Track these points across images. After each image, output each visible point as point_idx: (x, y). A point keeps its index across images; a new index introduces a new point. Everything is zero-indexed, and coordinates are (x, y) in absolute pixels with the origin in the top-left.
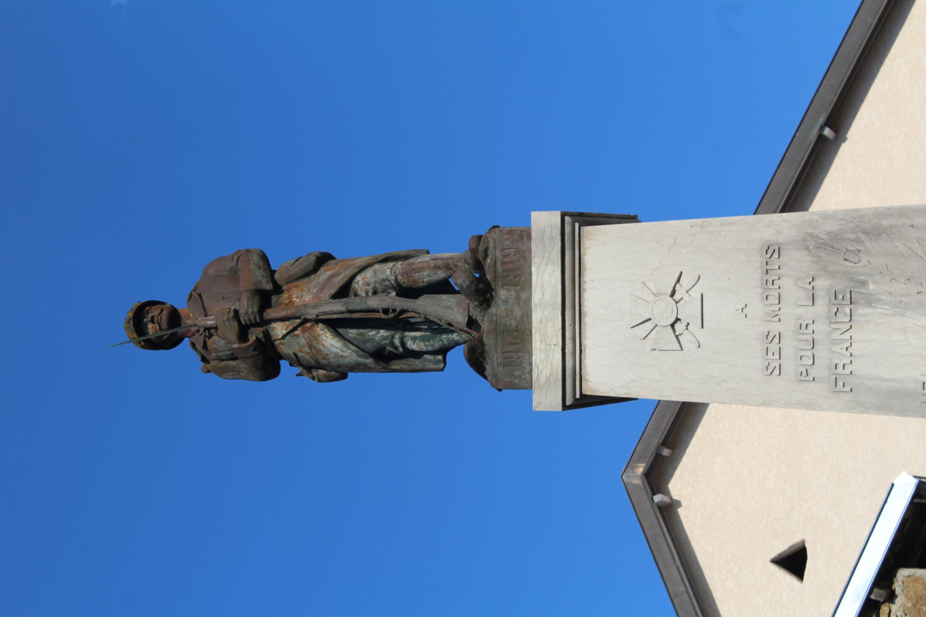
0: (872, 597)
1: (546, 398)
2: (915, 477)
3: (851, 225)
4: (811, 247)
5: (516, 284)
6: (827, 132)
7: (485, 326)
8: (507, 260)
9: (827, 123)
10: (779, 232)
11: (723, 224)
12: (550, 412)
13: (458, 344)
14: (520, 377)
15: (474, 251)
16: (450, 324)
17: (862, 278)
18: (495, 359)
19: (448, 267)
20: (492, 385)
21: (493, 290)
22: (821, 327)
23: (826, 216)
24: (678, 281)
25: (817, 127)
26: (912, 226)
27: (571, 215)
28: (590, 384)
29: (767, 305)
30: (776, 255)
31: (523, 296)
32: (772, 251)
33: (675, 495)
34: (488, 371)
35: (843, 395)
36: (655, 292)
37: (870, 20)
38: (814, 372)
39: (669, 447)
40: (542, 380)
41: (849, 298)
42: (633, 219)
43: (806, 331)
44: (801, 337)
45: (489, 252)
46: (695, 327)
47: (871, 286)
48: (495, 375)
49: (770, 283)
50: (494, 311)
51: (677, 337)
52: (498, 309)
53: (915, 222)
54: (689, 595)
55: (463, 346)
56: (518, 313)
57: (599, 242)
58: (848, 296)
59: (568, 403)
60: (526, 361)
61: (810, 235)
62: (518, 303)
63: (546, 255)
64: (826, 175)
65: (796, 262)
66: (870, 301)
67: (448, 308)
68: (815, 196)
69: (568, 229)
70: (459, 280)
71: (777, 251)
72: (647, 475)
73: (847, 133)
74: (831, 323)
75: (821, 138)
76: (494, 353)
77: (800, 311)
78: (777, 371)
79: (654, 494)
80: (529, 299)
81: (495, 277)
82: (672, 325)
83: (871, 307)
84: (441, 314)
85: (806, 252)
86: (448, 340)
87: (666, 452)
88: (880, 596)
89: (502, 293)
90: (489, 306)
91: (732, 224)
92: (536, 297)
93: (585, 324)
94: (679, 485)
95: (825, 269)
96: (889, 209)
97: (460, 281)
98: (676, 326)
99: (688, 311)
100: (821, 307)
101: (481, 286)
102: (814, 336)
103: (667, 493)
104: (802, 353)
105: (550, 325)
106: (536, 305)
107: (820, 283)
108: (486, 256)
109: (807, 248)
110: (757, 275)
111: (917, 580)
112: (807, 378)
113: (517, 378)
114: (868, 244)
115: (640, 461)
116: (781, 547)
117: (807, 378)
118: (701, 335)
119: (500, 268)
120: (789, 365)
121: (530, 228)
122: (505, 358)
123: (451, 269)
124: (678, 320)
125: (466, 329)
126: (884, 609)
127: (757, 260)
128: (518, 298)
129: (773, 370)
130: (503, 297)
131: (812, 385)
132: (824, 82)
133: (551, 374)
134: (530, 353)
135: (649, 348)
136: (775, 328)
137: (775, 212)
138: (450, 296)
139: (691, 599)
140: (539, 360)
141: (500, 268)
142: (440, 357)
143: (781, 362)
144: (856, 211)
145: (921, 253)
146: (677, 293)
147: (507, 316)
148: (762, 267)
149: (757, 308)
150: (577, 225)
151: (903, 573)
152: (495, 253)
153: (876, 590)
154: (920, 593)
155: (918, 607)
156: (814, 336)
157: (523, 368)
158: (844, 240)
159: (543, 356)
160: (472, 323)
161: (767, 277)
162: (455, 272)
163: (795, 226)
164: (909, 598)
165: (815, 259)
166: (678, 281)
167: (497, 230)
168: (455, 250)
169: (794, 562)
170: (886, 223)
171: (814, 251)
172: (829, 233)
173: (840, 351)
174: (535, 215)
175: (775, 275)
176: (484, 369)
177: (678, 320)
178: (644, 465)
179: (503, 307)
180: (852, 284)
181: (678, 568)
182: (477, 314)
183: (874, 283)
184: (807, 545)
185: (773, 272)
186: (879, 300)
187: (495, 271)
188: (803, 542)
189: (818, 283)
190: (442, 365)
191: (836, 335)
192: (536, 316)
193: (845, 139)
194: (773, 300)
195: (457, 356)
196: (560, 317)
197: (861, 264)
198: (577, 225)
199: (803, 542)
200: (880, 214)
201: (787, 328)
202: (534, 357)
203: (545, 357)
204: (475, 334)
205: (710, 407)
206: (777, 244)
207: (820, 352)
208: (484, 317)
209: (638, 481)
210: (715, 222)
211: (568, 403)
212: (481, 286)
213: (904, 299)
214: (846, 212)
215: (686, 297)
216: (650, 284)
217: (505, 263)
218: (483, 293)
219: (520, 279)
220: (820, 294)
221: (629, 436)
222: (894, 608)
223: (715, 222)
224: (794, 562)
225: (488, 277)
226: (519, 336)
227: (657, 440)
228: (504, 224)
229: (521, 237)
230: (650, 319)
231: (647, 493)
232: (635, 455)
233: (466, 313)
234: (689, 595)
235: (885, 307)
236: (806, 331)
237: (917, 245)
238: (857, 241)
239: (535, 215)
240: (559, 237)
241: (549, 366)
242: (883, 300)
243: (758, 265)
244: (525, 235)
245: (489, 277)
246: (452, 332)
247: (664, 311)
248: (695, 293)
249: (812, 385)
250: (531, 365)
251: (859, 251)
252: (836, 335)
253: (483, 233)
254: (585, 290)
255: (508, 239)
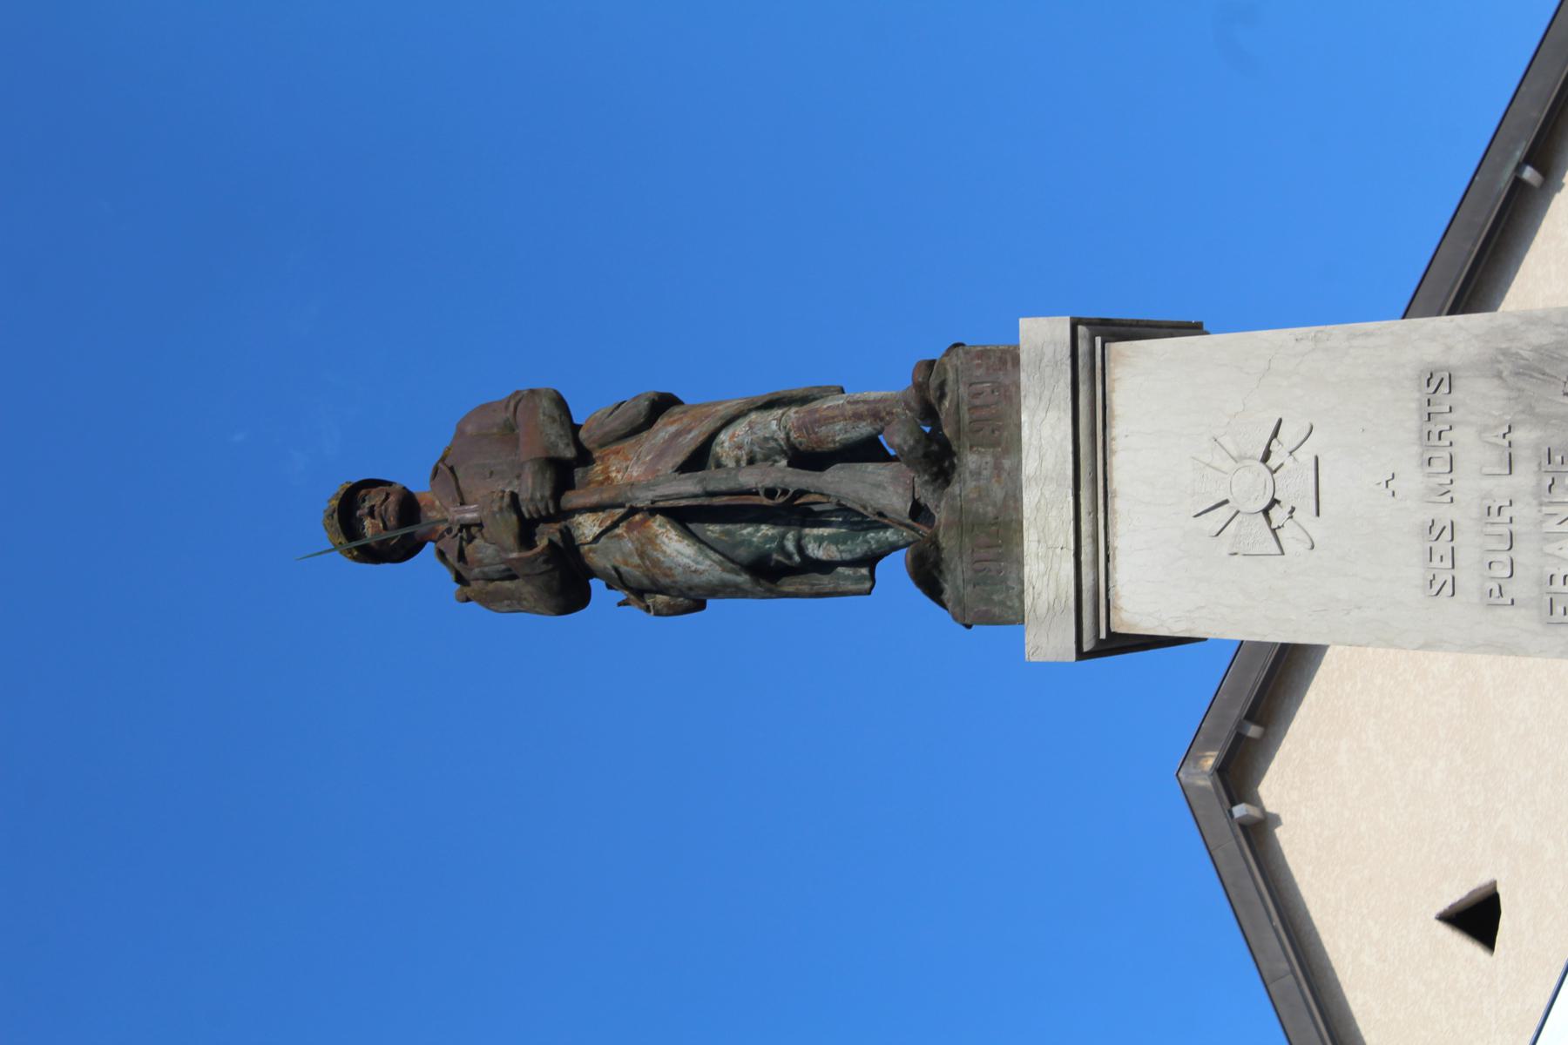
4: (1505, 374)
6: (1529, 174)
10: (1449, 348)
11: (1353, 336)
22: (1525, 512)
25: (1511, 167)
27: (1088, 323)
28: (1124, 615)
30: (1444, 388)
33: (1270, 805)
36: (1235, 454)
38: (1513, 589)
39: (1258, 723)
42: (1195, 328)
43: (1498, 519)
44: (1489, 529)
49: (1434, 436)
51: (1274, 531)
54: (1296, 977)
57: (1137, 370)
59: (1086, 647)
61: (1505, 353)
65: (1480, 400)
69: (1083, 347)
71: (1446, 381)
72: (1222, 770)
74: (1541, 504)
75: (1518, 184)
77: (1488, 484)
78: (1448, 589)
79: (1233, 803)
82: (1266, 512)
85: (1496, 382)
87: (1253, 731)
91: (1367, 334)
94: (1276, 788)
95: (1530, 410)
99: (1294, 486)
100: (1526, 477)
102: (1514, 527)
103: (1255, 801)
104: (1491, 557)
105: (1054, 513)
109: (1499, 376)
112: (1501, 601)
116: (1456, 892)
117: (1501, 601)
120: (1469, 579)
124: (1274, 502)
127: (1412, 399)
129: (1442, 588)
131: (1509, 612)
135: (1225, 551)
136: (1445, 514)
137: (1439, 314)
139: (1299, 985)
143: (1454, 572)
149: (1413, 480)
150: (1098, 340)
161: (1430, 426)
163: (1477, 336)
165: (1514, 394)
177: (1274, 502)
178: (1215, 753)
181: (1276, 931)
184: (1501, 890)
185: (1439, 417)
188: (1494, 884)
193: (1559, 187)
194: (1441, 466)
196: (1071, 499)
198: (1098, 340)
199: (1494, 884)
201: (1464, 513)
205: (1329, 652)
207: (1523, 554)
209: (1205, 782)
211: (1086, 647)
215: (1289, 462)
220: (1521, 454)
224: (1478, 918)
227: (1237, 711)
230: (1226, 502)
231: (1221, 802)
232: (1200, 737)
234: (1296, 977)
236: (1498, 519)
240: (1069, 362)
241: (1052, 585)
243: (1413, 405)
247: (1251, 488)
248: (1305, 456)
252: (1552, 525)
254: (1113, 453)
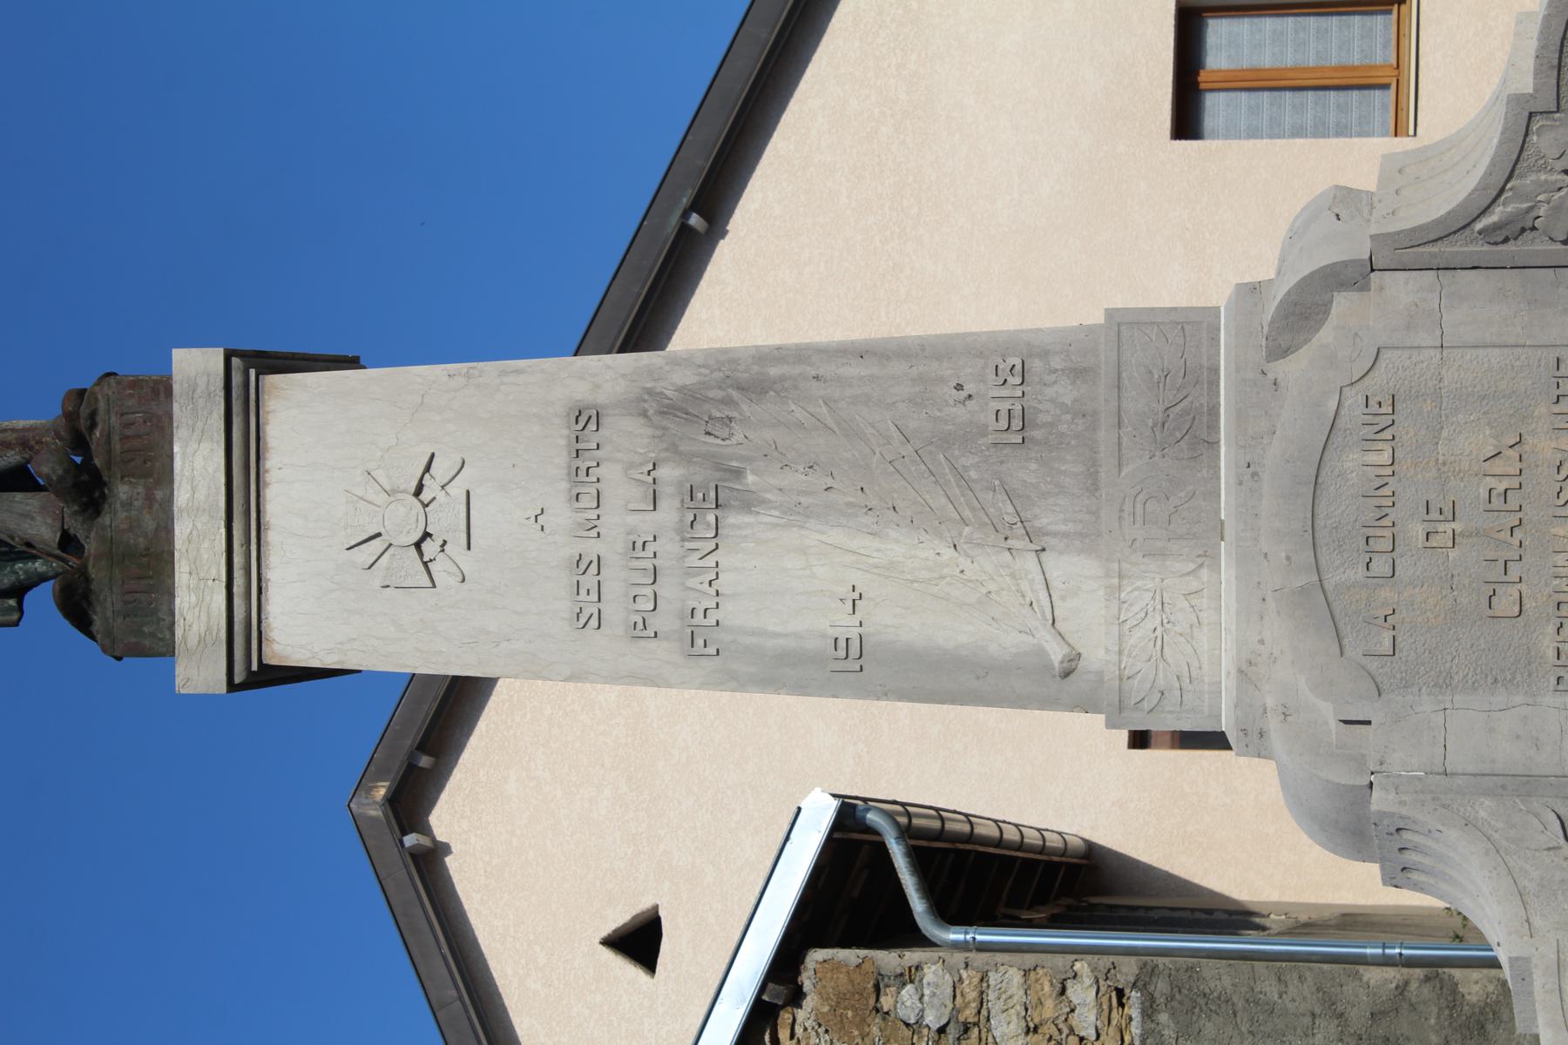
0: (765, 997)
1: (200, 670)
2: (834, 796)
3: (718, 375)
4: (651, 412)
5: (146, 475)
6: (695, 220)
7: (91, 547)
8: (129, 432)
9: (694, 207)
10: (597, 386)
11: (504, 373)
12: (205, 696)
13: (43, 578)
14: (152, 635)
15: (70, 416)
16: (29, 545)
17: (734, 464)
18: (109, 604)
19: (24, 444)
20: (105, 651)
21: (105, 484)
22: (668, 547)
23: (677, 361)
24: (428, 469)
25: (678, 213)
26: (816, 378)
28: (276, 647)
29: (578, 510)
31: (159, 494)
32: (585, 418)
33: (441, 834)
34: (98, 625)
35: (703, 661)
36: (388, 488)
37: (766, 35)
38: (655, 623)
39: (430, 754)
40: (192, 640)
41: (715, 497)
42: (352, 363)
45: (98, 419)
46: (456, 548)
47: (750, 478)
48: (109, 633)
49: (582, 473)
50: (108, 522)
51: (425, 564)
52: (114, 518)
53: (821, 372)
54: (463, 1003)
55: (52, 582)
56: (149, 523)
57: (291, 402)
58: (713, 494)
59: (237, 680)
60: (165, 607)
61: (650, 392)
62: (150, 507)
63: (199, 424)
64: (692, 293)
65: (626, 438)
66: (749, 503)
67: (27, 516)
68: (675, 327)
69: (237, 379)
70: (45, 467)
71: (594, 419)
72: (392, 800)
73: (727, 223)
74: (683, 540)
75: (684, 230)
76: (113, 595)
77: (633, 519)
78: (594, 622)
79: (404, 833)
80: (170, 499)
81: (109, 463)
83: (750, 512)
84: (12, 526)
85: (642, 420)
86: (26, 572)
87: (425, 761)
88: (778, 996)
89: (122, 491)
90: (98, 513)
91: (518, 372)
92: (181, 497)
93: (267, 543)
95: (673, 448)
96: (779, 348)
97: (45, 470)
98: (424, 546)
99: (445, 520)
100: (669, 512)
101: (85, 477)
103: (426, 830)
105: (206, 545)
106: (181, 511)
107: (667, 473)
108: (93, 425)
109: (644, 414)
110: (561, 458)
111: (838, 966)
112: (645, 633)
113: (145, 633)
114: (744, 407)
115: (380, 777)
116: (619, 917)
117: (645, 633)
118: (466, 561)
119: (117, 447)
120: (615, 611)
121: (170, 378)
122: (126, 603)
123: (31, 448)
124: (427, 535)
125: (58, 552)
126: (785, 1016)
128: (149, 498)
129: (588, 620)
130: (123, 497)
131: (653, 644)
132: (689, 137)
133: (208, 629)
134: (171, 595)
135: (378, 583)
136: (592, 548)
137: (609, 352)
138: (29, 495)
139: (467, 1011)
140: (186, 605)
141: (118, 447)
142: (12, 602)
144: (725, 351)
145: (830, 422)
146: (425, 490)
147: (131, 529)
148: (569, 445)
149: (561, 515)
150: (252, 372)
151: (816, 956)
152: (109, 420)
153: (771, 986)
154: (842, 989)
155: (839, 1011)
156: (655, 561)
157: (160, 620)
158: (706, 400)
159: (193, 598)
160: (68, 542)
161: (578, 463)
162: (37, 453)
164: (824, 998)
165: (659, 433)
166: (428, 469)
167: (112, 380)
168: (38, 412)
169: (639, 942)
170: (774, 371)
171: (656, 419)
172: (680, 389)
173: (699, 587)
174: (178, 354)
175: (591, 459)
176: (90, 623)
177: (427, 535)
178: (386, 784)
179: (122, 515)
180: (718, 475)
182: (76, 526)
183: (754, 473)
184: (662, 914)
185: (587, 454)
186: (763, 502)
187: (109, 452)
188: (656, 908)
189: (663, 472)
190: (15, 617)
191: (693, 560)
192: (182, 530)
193: (724, 234)
194: (588, 501)
195: (42, 600)
196: (223, 531)
197: (734, 440)
198: (252, 372)
199: (656, 908)
200: (766, 356)
201: (610, 548)
202: (178, 601)
203: (197, 602)
204: (74, 561)
205: (500, 683)
206: (595, 406)
207: (667, 589)
208: (89, 531)
209: (376, 812)
210: (490, 368)
211: (237, 680)
212: (85, 477)
213: (802, 500)
214: (708, 353)
215: (441, 496)
216: (378, 474)
217: (128, 437)
218: (87, 489)
219: (154, 467)
220: (665, 490)
221: (363, 731)
222: (801, 1014)
223: (489, 370)
224: (639, 942)
225: (97, 461)
226: (152, 564)
227: (409, 742)
228: (126, 369)
229: (155, 392)
230: (379, 535)
231: (391, 829)
232: (372, 768)
233: (58, 525)
234: (463, 1003)
235: (773, 512)
236: (642, 554)
237: (824, 410)
238: (728, 402)
239: (178, 354)
240: (222, 394)
241: (204, 618)
242: (770, 501)
243: (563, 442)
244: (162, 388)
245: (97, 462)
246: (34, 558)
247: (403, 521)
248: (457, 490)
249: (653, 645)
250: (173, 614)
251: (730, 419)
252: (693, 560)
253: (87, 383)
254: (266, 484)
255: (131, 396)
